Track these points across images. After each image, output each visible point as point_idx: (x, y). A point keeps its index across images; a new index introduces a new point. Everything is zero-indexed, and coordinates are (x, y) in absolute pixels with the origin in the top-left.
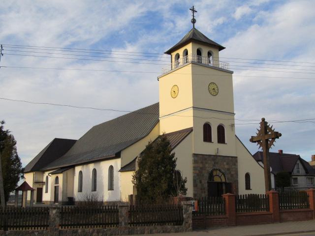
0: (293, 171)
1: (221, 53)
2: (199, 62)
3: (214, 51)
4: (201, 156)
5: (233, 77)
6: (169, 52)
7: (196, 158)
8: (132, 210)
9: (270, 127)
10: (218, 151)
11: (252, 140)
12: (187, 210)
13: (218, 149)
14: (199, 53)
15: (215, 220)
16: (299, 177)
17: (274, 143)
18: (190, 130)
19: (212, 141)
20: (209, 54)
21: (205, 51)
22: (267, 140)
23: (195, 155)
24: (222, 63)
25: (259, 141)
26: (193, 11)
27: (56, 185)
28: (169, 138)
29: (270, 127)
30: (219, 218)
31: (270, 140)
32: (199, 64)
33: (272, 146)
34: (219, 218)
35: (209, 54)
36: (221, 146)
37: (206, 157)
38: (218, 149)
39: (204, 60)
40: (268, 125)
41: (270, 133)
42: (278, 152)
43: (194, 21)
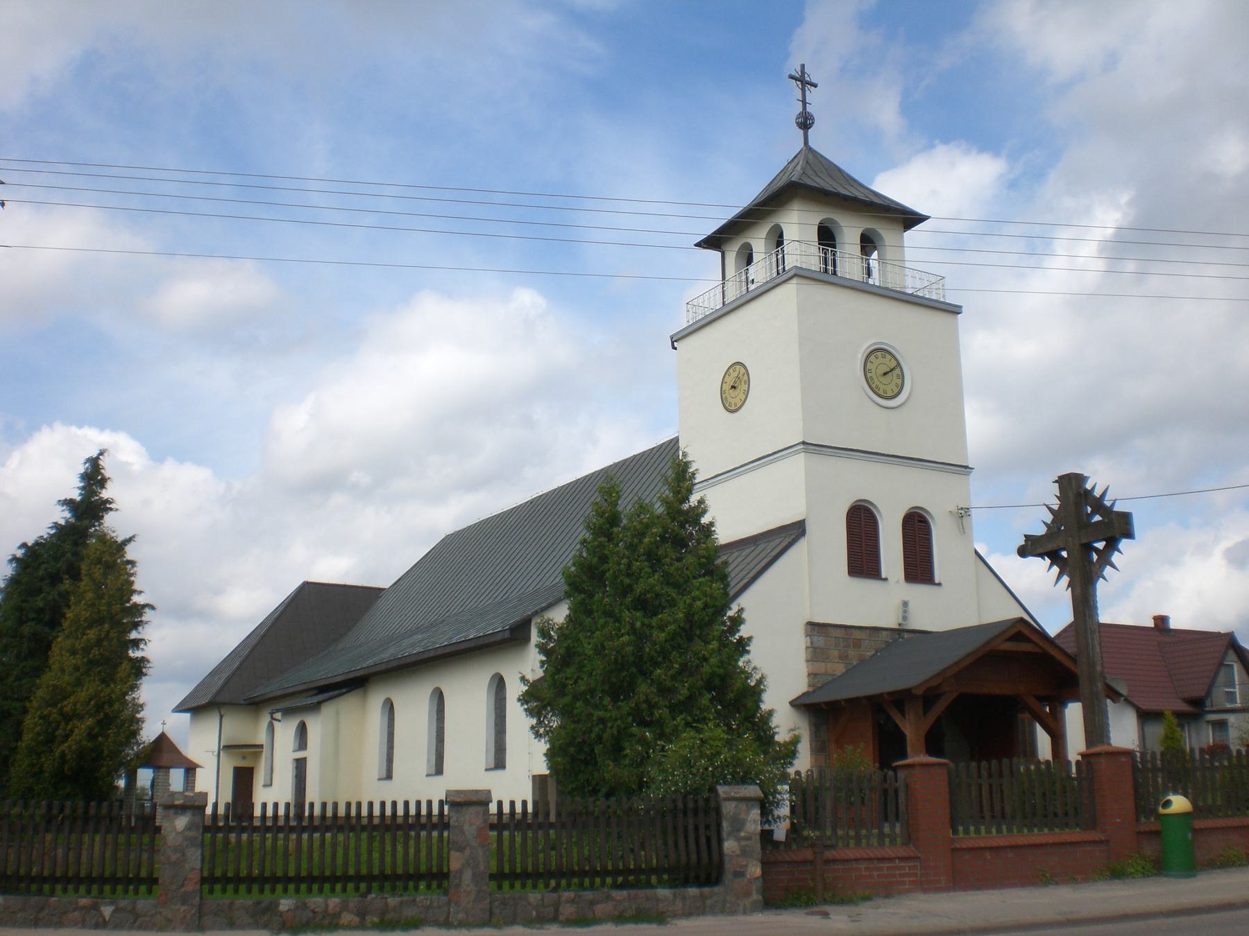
0: (1209, 693)
1: (912, 236)
2: (826, 271)
3: (887, 234)
4: (840, 633)
5: (964, 339)
6: (714, 242)
7: (820, 641)
8: (541, 819)
9: (1097, 493)
10: (905, 611)
11: (1029, 548)
12: (738, 824)
13: (905, 604)
14: (827, 236)
15: (862, 866)
16: (1232, 719)
17: (1116, 558)
18: (796, 531)
19: (883, 576)
20: (868, 243)
21: (850, 231)
22: (1088, 548)
23: (814, 628)
24: (917, 275)
25: (1054, 557)
26: (803, 81)
27: (300, 755)
28: (810, 671)
29: (1097, 493)
30: (882, 859)
31: (1100, 545)
32: (824, 277)
33: (1108, 570)
34: (882, 859)
35: (868, 243)
36: (918, 592)
37: (857, 635)
38: (905, 604)
39: (849, 262)
40: (1088, 486)
41: (1097, 518)
42: (1151, 624)
43: (805, 123)
